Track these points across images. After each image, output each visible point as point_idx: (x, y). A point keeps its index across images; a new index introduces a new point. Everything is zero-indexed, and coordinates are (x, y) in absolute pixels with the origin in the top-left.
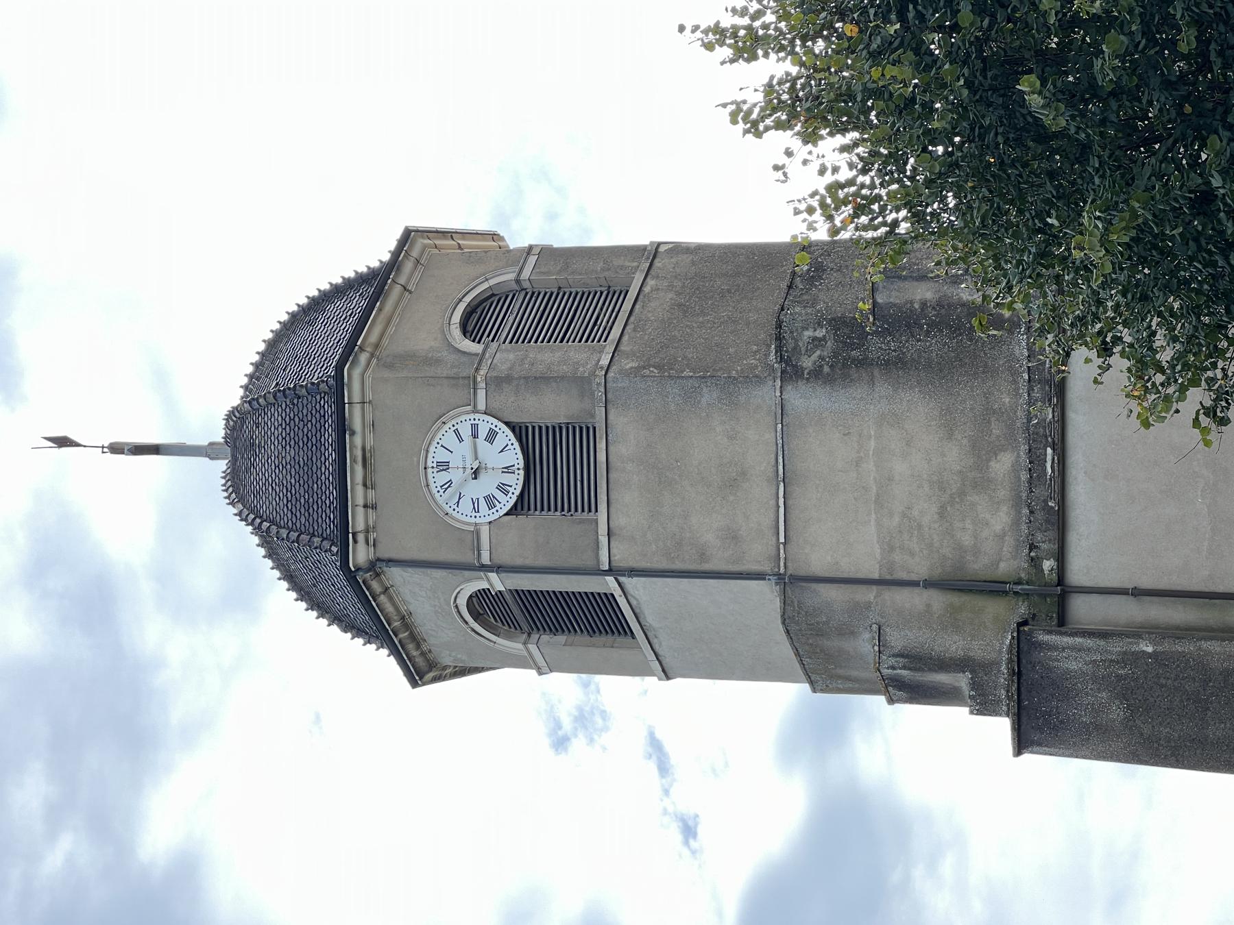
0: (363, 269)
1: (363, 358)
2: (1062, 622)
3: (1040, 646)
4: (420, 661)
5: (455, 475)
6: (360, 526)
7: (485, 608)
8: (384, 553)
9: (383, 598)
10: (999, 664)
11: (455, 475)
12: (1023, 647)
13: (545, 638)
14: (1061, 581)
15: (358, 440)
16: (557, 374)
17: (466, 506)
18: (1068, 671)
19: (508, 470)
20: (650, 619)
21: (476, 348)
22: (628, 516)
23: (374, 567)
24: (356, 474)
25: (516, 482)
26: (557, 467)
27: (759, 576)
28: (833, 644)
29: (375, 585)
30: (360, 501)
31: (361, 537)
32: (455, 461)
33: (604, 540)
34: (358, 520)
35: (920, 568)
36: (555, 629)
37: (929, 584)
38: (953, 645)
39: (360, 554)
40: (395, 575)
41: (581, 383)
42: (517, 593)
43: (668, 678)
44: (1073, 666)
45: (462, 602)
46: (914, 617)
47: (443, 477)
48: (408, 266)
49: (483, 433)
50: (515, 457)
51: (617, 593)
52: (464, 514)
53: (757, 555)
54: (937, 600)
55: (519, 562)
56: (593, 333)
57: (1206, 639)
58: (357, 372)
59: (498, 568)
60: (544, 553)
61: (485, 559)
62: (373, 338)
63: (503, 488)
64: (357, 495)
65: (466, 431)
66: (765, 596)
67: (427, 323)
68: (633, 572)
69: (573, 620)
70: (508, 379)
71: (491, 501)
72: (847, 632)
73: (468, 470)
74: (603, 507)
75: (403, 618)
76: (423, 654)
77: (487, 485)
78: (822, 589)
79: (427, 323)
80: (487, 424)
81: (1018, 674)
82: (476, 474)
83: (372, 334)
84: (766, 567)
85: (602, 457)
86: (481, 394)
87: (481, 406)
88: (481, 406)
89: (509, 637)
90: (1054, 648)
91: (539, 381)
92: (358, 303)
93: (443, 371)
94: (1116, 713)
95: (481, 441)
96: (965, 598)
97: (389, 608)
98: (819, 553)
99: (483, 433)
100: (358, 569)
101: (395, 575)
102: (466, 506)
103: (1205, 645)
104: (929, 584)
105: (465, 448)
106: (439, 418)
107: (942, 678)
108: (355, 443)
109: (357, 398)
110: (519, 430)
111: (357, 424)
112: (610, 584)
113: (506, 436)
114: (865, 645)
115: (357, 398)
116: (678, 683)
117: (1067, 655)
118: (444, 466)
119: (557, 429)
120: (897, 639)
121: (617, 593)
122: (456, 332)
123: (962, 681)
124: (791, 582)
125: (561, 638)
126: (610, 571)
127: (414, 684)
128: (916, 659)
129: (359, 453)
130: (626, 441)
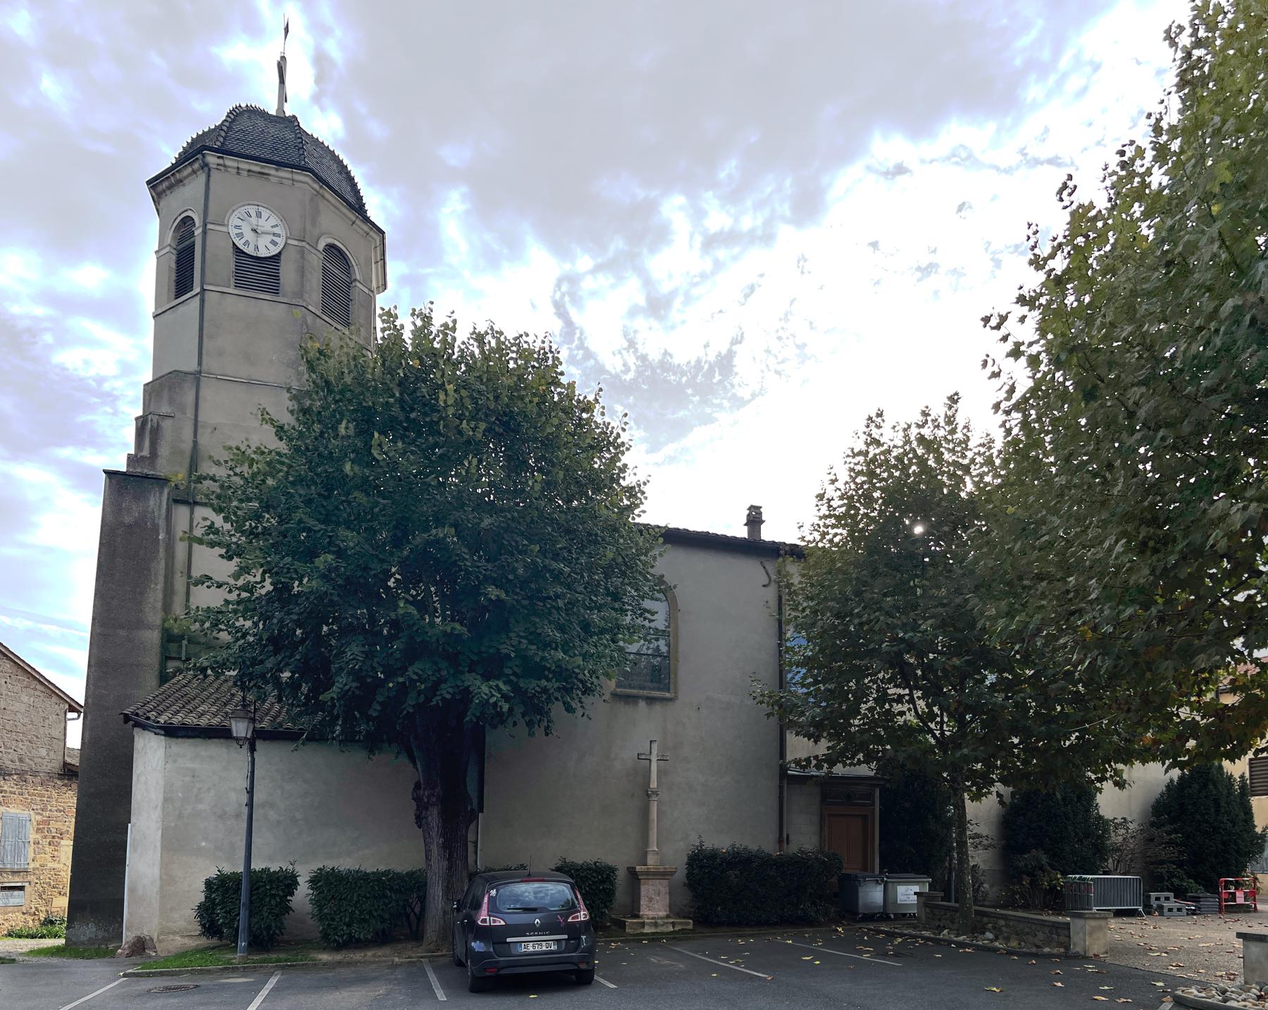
0: (367, 207)
1: (316, 186)
2: (176, 501)
3: (162, 488)
4: (160, 188)
5: (254, 220)
6: (228, 163)
7: (187, 221)
8: (213, 173)
9: (190, 170)
10: (154, 469)
11: (254, 220)
12: (162, 481)
13: (174, 258)
14: (196, 503)
15: (273, 172)
16: (304, 279)
17: (239, 222)
18: (148, 499)
19: (257, 248)
20: (181, 309)
21: (321, 246)
22: (232, 306)
23: (205, 165)
24: (256, 167)
25: (250, 250)
26: (258, 273)
27: (200, 363)
28: (165, 394)
29: (196, 166)
30: (241, 166)
31: (221, 161)
32: (262, 221)
33: (219, 289)
34: (231, 162)
35: (203, 440)
36: (178, 262)
37: (195, 443)
38: (164, 451)
39: (212, 159)
40: (202, 178)
41: (300, 294)
42: (193, 246)
43: (155, 317)
44: (152, 503)
45: (189, 213)
46: (177, 435)
47: (253, 214)
48: (365, 228)
49: (275, 239)
50: (263, 253)
51: (193, 293)
52: (234, 221)
53: (210, 363)
54: (187, 446)
55: (208, 243)
56: (326, 308)
57: (167, 564)
58: (307, 180)
59: (205, 232)
60: (215, 264)
61: (209, 226)
62: (327, 195)
63: (247, 243)
64: (245, 165)
65: (277, 230)
66: (193, 366)
67: (333, 226)
68: (202, 301)
69: (182, 272)
70: (303, 257)
71: (240, 235)
72: (171, 401)
73: (257, 226)
74: (236, 292)
75: (181, 181)
76: (164, 191)
77: (248, 235)
78: (193, 393)
79: (333, 226)
80: (281, 242)
81: (146, 477)
82: (255, 231)
83: (329, 195)
84: (205, 367)
85: (262, 296)
86: (296, 243)
87: (290, 241)
88: (290, 241)
89: (173, 238)
90: (161, 493)
91: (302, 272)
92: (352, 200)
93: (308, 227)
94: (128, 520)
95: (272, 237)
96: (188, 460)
97: (185, 173)
98: (209, 392)
99: (275, 239)
100: (204, 156)
101: (202, 178)
102: (239, 222)
103: (163, 563)
104: (195, 443)
105: (268, 228)
106: (284, 219)
107: (147, 443)
108: (270, 170)
109: (296, 177)
110: (276, 258)
111: (281, 174)
112: (197, 290)
113: (274, 251)
114: (165, 409)
115: (296, 177)
116: (152, 321)
117: (157, 502)
118: (259, 215)
119: (277, 277)
120: (167, 425)
121: (193, 293)
122: (330, 241)
123: (146, 453)
124: (197, 376)
125: (174, 265)
126: (203, 290)
127: (148, 183)
128: (156, 433)
129: (266, 171)
130: (265, 309)
